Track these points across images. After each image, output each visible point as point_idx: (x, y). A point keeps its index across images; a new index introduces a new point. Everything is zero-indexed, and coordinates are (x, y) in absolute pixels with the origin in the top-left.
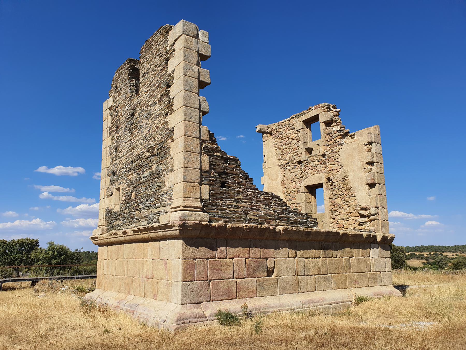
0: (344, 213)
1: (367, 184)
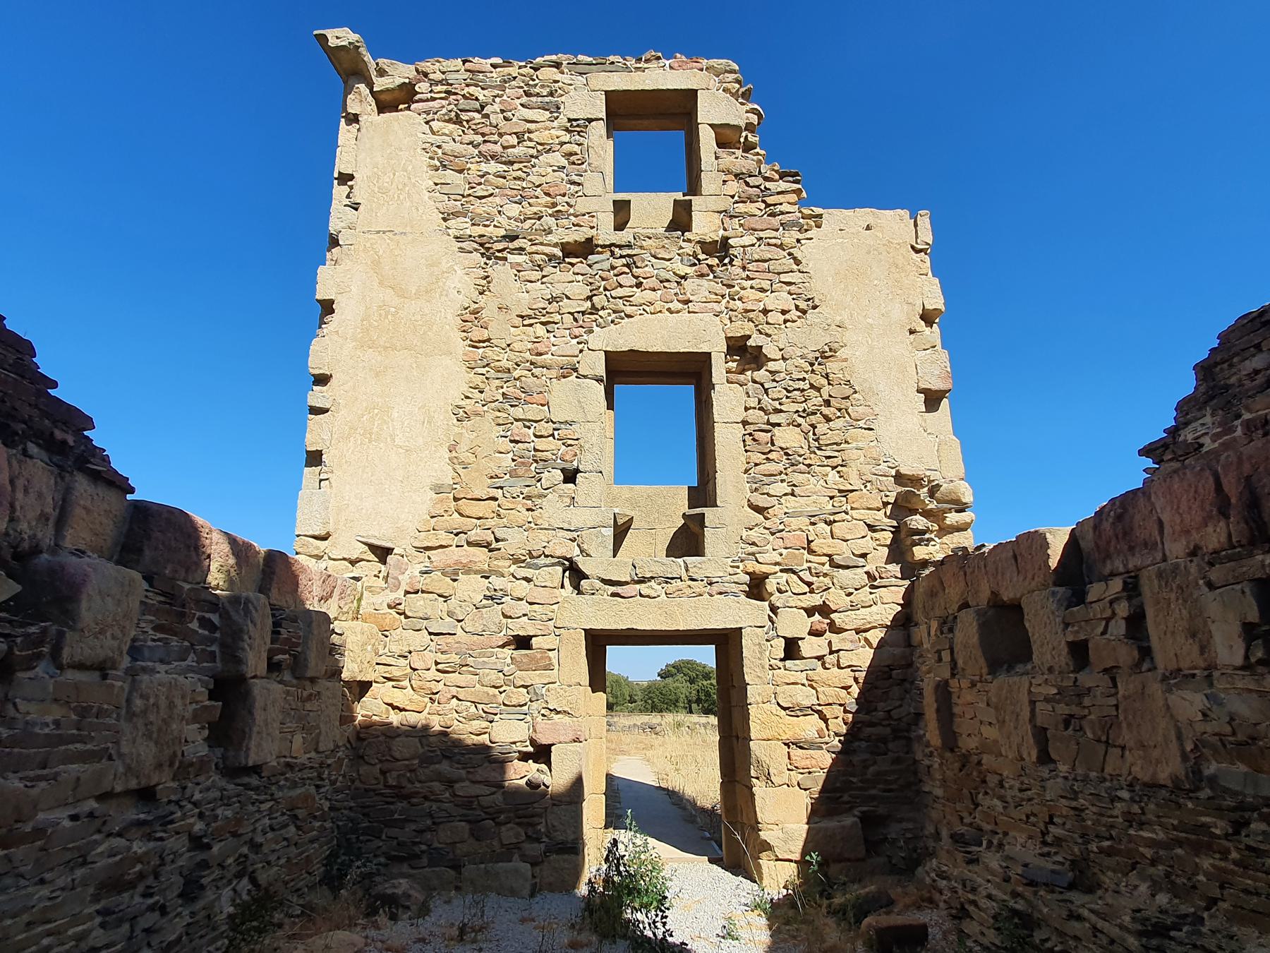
0: (816, 490)
1: (918, 391)
